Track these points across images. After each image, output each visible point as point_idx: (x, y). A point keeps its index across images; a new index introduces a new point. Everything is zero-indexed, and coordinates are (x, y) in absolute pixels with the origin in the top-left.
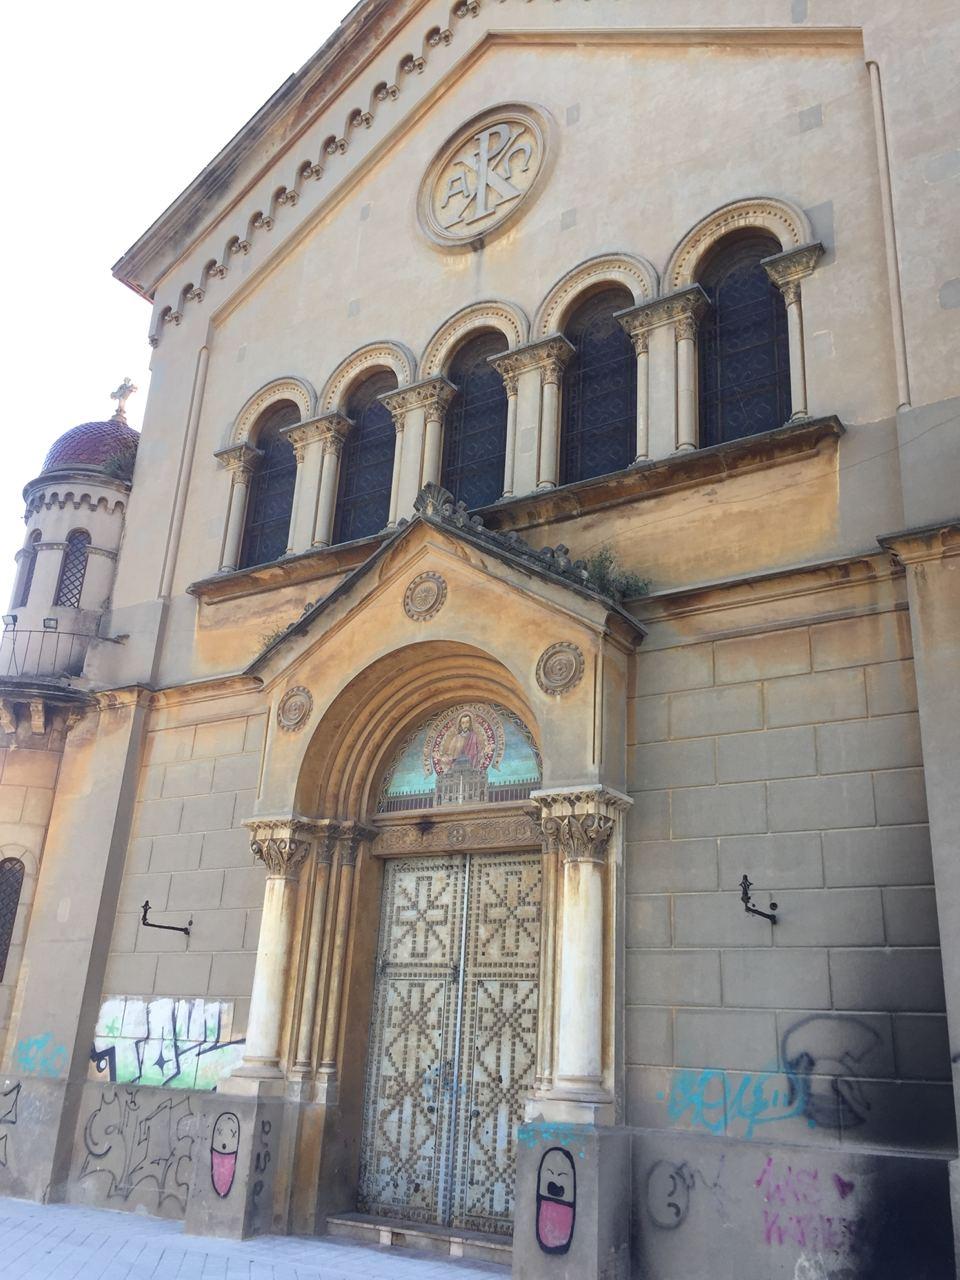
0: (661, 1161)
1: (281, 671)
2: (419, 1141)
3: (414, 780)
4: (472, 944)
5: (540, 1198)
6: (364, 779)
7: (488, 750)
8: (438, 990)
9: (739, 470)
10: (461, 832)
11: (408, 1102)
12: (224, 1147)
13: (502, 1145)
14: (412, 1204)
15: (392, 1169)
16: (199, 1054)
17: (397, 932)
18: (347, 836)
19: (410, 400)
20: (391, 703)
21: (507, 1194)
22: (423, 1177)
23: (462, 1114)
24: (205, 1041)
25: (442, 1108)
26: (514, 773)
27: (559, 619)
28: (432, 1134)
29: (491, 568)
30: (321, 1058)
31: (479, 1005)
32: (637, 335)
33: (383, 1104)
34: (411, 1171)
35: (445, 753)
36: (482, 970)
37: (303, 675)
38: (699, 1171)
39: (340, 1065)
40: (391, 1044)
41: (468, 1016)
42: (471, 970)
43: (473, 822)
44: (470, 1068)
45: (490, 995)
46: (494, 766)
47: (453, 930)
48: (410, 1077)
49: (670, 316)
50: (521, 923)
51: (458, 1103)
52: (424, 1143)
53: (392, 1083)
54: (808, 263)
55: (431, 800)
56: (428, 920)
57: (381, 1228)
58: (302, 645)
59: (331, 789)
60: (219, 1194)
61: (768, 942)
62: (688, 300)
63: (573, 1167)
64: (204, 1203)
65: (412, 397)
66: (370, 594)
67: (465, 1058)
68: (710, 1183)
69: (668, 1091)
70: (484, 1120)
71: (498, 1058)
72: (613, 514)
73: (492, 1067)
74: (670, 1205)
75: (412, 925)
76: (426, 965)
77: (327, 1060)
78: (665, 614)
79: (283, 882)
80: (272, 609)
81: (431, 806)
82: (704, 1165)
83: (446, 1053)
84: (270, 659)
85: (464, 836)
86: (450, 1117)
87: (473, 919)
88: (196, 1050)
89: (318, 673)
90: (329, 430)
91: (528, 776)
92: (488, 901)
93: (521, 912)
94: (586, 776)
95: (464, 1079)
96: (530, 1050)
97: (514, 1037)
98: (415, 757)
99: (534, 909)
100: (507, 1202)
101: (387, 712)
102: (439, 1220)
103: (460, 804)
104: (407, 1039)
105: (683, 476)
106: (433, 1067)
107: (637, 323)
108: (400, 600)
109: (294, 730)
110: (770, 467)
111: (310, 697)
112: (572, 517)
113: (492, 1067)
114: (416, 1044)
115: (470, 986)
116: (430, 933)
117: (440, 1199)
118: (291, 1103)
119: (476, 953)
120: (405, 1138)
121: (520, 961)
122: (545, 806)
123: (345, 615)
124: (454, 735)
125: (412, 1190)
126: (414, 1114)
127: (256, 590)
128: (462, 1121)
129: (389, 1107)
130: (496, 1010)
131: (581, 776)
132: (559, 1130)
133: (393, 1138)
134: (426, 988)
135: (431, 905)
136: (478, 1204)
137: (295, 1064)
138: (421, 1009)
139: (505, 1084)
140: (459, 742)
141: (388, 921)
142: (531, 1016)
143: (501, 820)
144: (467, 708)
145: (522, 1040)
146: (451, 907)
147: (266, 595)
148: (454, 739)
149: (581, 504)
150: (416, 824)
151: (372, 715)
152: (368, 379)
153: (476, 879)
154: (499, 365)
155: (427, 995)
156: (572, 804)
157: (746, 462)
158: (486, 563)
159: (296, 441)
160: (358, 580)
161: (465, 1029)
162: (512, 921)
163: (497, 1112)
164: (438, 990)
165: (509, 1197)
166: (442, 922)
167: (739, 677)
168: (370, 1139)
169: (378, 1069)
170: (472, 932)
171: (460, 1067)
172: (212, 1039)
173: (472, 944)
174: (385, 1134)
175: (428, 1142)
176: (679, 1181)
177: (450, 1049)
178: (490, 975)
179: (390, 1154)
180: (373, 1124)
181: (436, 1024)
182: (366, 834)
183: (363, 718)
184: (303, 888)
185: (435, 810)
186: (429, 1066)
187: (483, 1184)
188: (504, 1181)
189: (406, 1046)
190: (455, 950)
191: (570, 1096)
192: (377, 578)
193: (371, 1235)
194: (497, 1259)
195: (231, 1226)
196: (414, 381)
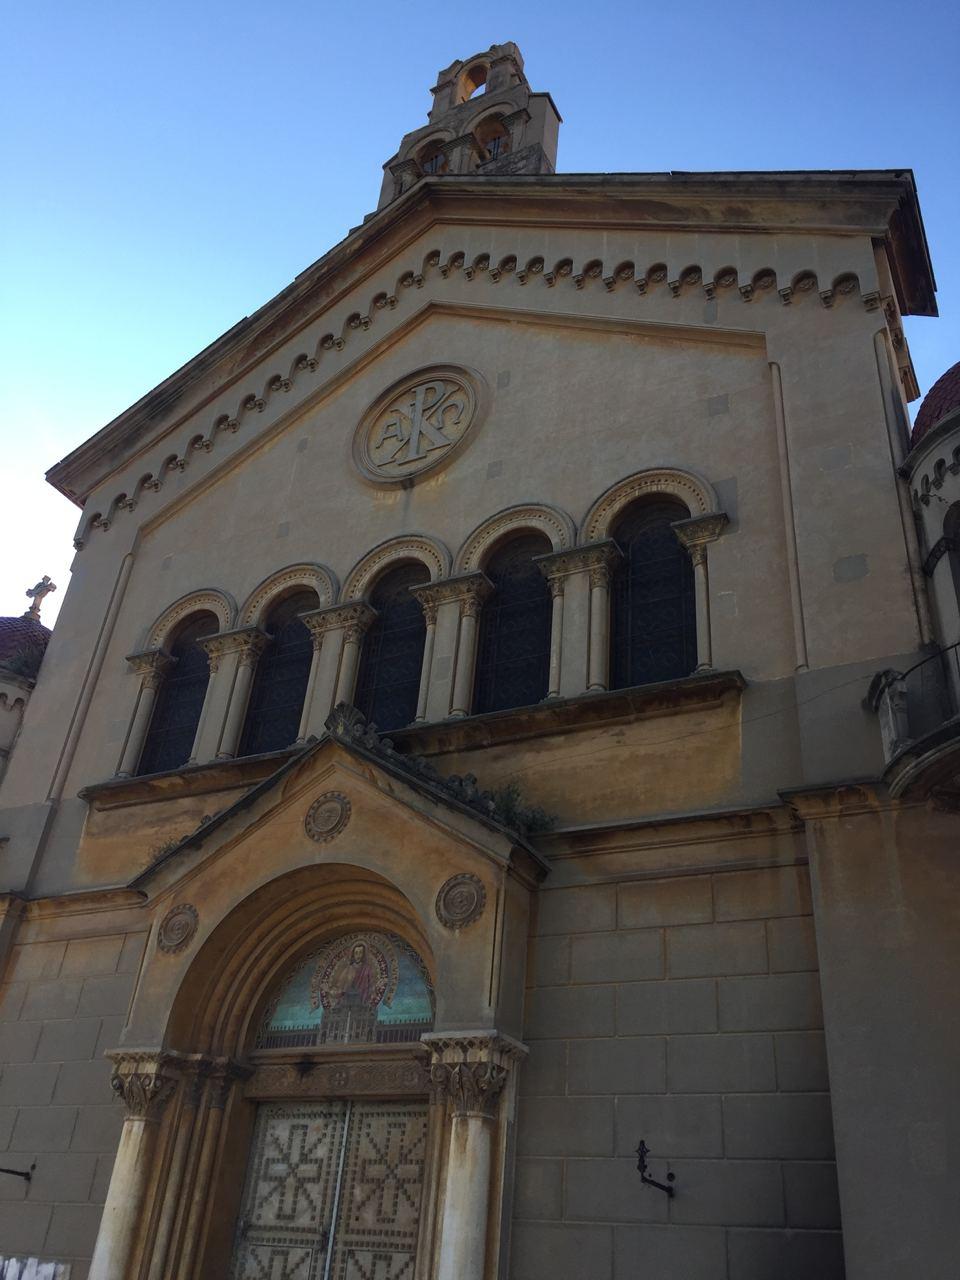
3: (299, 1015)
4: (345, 1206)
7: (380, 984)
8: (303, 1260)
10: (344, 1075)
17: (264, 1188)
18: (218, 1075)
35: (334, 985)
36: (354, 1238)
37: (192, 890)
42: (341, 1236)
43: (358, 1064)
47: (326, 1188)
50: (400, 1184)
54: (714, 530)
55: (315, 1036)
58: (199, 857)
62: (603, 551)
76: (292, 1229)
80: (168, 819)
81: (314, 1044)
87: (349, 1177)
90: (246, 642)
91: (421, 1015)
103: (346, 1043)
107: (554, 569)
110: (676, 714)
115: (339, 1256)
119: (349, 1217)
124: (345, 966)
140: (350, 975)
141: (254, 1175)
143: (387, 1064)
144: (362, 937)
146: (325, 1162)
150: (296, 1064)
151: (260, 940)
154: (420, 595)
155: (291, 1265)
159: (211, 651)
164: (303, 1260)
166: (314, 1179)
170: (347, 1192)
183: (251, 941)
185: (318, 1048)
190: (326, 1213)
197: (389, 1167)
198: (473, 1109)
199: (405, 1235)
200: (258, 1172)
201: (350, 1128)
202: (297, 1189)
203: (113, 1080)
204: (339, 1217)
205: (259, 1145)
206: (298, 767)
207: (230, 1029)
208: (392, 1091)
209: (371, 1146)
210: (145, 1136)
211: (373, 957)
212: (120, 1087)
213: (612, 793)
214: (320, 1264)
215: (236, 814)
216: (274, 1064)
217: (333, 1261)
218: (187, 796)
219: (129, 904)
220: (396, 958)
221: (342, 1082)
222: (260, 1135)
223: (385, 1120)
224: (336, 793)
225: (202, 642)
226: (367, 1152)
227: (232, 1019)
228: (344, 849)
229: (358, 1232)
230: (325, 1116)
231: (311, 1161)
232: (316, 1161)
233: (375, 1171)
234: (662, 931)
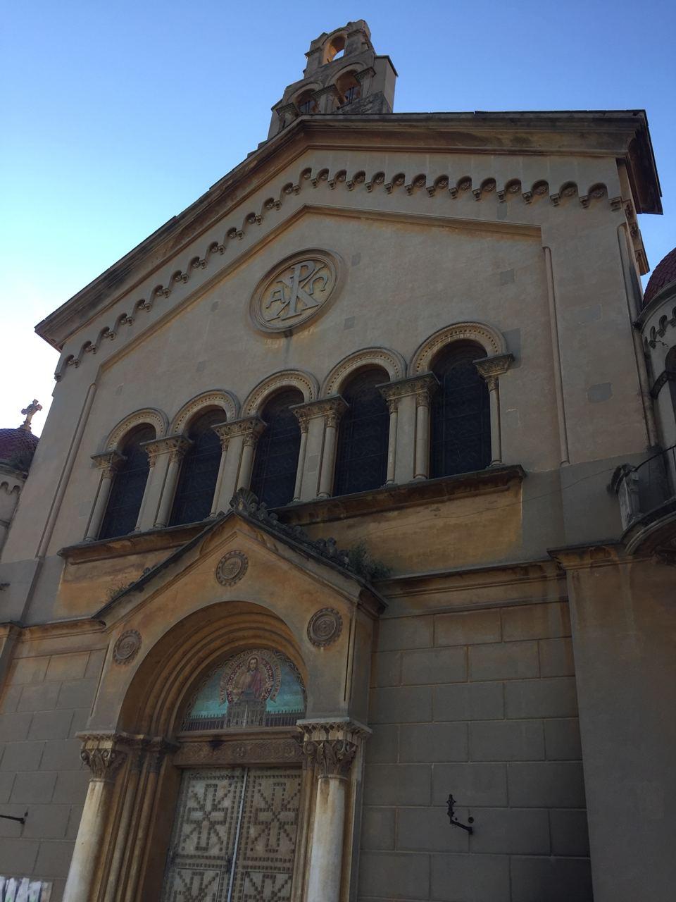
3: (212, 707)
4: (243, 842)
6: (173, 704)
7: (268, 685)
10: (243, 749)
17: (187, 828)
29: (281, 551)
31: (245, 892)
32: (391, 400)
35: (236, 686)
36: (250, 863)
42: (241, 862)
43: (253, 742)
46: (271, 699)
49: (413, 391)
50: (282, 825)
54: (503, 365)
58: (139, 598)
76: (207, 857)
81: (222, 727)
87: (246, 820)
90: (175, 446)
91: (296, 707)
107: (391, 393)
110: (476, 495)
112: (339, 519)
115: (239, 876)
119: (246, 849)
121: (279, 857)
141: (180, 819)
146: (229, 811)
150: (209, 741)
151: (185, 654)
152: (206, 414)
153: (251, 788)
154: (297, 412)
155: (205, 882)
170: (244, 831)
173: (243, 842)
182: (171, 748)
183: (177, 657)
185: (225, 730)
197: (274, 814)
198: (333, 773)
200: (183, 817)
201: (247, 786)
202: (210, 829)
203: (82, 753)
204: (239, 849)
206: (210, 534)
210: (104, 793)
213: (430, 551)
215: (167, 567)
217: (235, 879)
218: (134, 554)
221: (242, 754)
229: (252, 859)
233: (263, 816)
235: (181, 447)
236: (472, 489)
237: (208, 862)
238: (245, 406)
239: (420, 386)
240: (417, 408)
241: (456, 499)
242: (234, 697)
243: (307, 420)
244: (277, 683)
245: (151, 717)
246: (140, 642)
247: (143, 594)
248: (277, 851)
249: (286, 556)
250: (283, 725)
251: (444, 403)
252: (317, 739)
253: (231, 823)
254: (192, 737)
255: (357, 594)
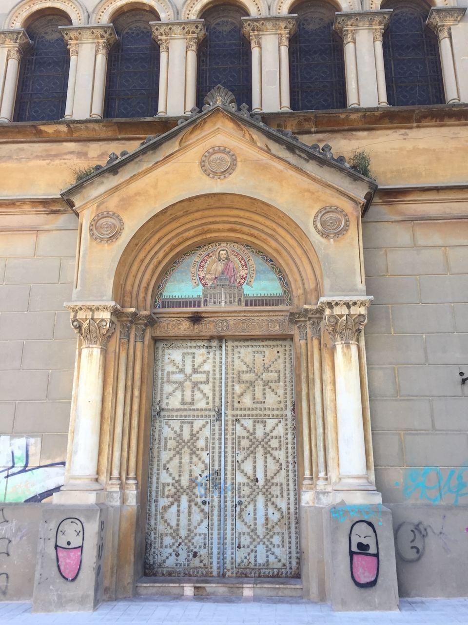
0: (404, 522)
1: (92, 197)
2: (195, 523)
3: (183, 287)
4: (229, 396)
5: (352, 554)
7: (243, 273)
8: (204, 426)
9: (421, 124)
10: (225, 324)
11: (184, 500)
12: (69, 543)
13: (261, 521)
14: (192, 565)
15: (173, 544)
16: (7, 477)
17: (168, 388)
18: (141, 322)
19: (175, 31)
20: (173, 234)
21: (267, 551)
22: (200, 547)
23: (229, 504)
24: (13, 467)
25: (212, 501)
26: (263, 289)
27: (329, 191)
28: (206, 518)
29: (273, 151)
30: (127, 474)
31: (237, 434)
32: (347, 30)
33: (163, 502)
34: (190, 544)
35: (208, 273)
36: (239, 412)
37: (112, 203)
38: (430, 526)
39: (140, 478)
40: (168, 462)
41: (229, 442)
42: (230, 412)
43: (235, 318)
44: (233, 474)
45: (245, 428)
46: (248, 284)
47: (214, 387)
48: (185, 482)
49: (371, 25)
50: (266, 383)
51: (225, 497)
52: (199, 525)
53: (170, 487)
54: (457, 17)
55: (199, 302)
56: (193, 380)
57: (184, 585)
58: (112, 181)
59: (128, 288)
60: (67, 579)
61: (460, 394)
62: (385, 18)
63: (375, 531)
64: (51, 587)
65: (178, 30)
66: (172, 154)
67: (229, 468)
68: (437, 532)
69: (402, 480)
70: (246, 507)
71: (255, 467)
72: (338, 135)
73: (250, 472)
74: (412, 548)
75: (181, 384)
76: (194, 410)
77: (132, 475)
78: (380, 201)
79: (99, 350)
80: (56, 156)
81: (199, 306)
82: (433, 522)
83: (213, 465)
84: (85, 188)
85: (228, 327)
86: (220, 506)
87: (230, 380)
88: (5, 474)
89: (127, 203)
90: (102, 37)
92: (240, 369)
93: (265, 376)
94: (357, 290)
95: (229, 482)
96: (278, 461)
97: (266, 453)
98: (184, 274)
99: (276, 375)
100: (267, 556)
101: (169, 241)
102: (215, 573)
103: (223, 307)
104: (181, 458)
105: (387, 120)
106: (204, 475)
107: (349, 23)
108: (197, 162)
109: (107, 242)
110: (442, 126)
111: (121, 220)
112: (309, 132)
113: (250, 472)
114: (188, 461)
115: (230, 423)
116: (196, 389)
117: (215, 560)
118: (112, 507)
119: (233, 402)
120: (184, 521)
121: (267, 407)
122: (329, 308)
123: (151, 165)
125: (191, 556)
126: (190, 507)
127: (40, 139)
128: (229, 508)
129: (169, 504)
130: (251, 437)
131: (353, 290)
132: (359, 509)
133: (173, 523)
134: (194, 425)
135: (195, 371)
136: (245, 560)
137: (111, 479)
138: (192, 439)
139: (261, 482)
140: (220, 267)
141: (160, 381)
142: (277, 440)
143: (256, 318)
145: (271, 455)
146: (211, 373)
147: (48, 144)
148: (215, 264)
149: (316, 125)
150: (188, 318)
151: (159, 240)
152: (128, 11)
153: (230, 355)
154: (249, 25)
155: (196, 429)
156: (348, 307)
157: (427, 120)
158: (270, 147)
159: (71, 39)
160: (165, 142)
161: (228, 450)
162: (260, 382)
163: (256, 501)
164: (204, 426)
165: (269, 553)
166: (205, 382)
167: (430, 243)
168: (153, 526)
169: (158, 479)
170: (230, 389)
171: (226, 474)
172: (20, 465)
173: (229, 396)
174: (166, 521)
175: (202, 524)
176: (416, 532)
177: (216, 463)
178: (245, 416)
179: (171, 534)
180: (156, 515)
181: (204, 448)
182: (151, 322)
183: (153, 241)
184: (111, 356)
185: (202, 309)
186: (200, 475)
187: (248, 547)
188: (264, 543)
189: (180, 463)
190: (217, 400)
191: (363, 488)
192: (177, 143)
193: (176, 591)
194: (280, 594)
195: (82, 601)
196: (178, 19)
197: (257, 375)
198: (352, 340)
199: (273, 409)
200: (162, 379)
201: (226, 354)
202: (193, 388)
203: (73, 322)
204: (226, 402)
205: (160, 364)
206: (193, 126)
207: (141, 295)
208: (260, 333)
209: (242, 363)
210: (101, 358)
211: (236, 259)
212: (79, 328)
213: (403, 169)
214: (217, 428)
215: (145, 153)
216: (172, 317)
217: (226, 425)
218: (71, 141)
219: (37, 211)
220: (251, 258)
221: (225, 328)
222: (160, 359)
223: (250, 350)
224: (222, 148)
225: (64, 30)
226: (240, 367)
227: (142, 289)
228: (236, 183)
229: (241, 409)
230: (207, 347)
231: (201, 372)
232: (204, 372)
233: (246, 377)
234: (443, 248)
235: (108, 40)
236: (438, 121)
237: (196, 413)
238: (184, 9)
239: (378, 22)
240: (187, 52)
241: (424, 127)
242: (207, 281)
243: (258, 35)
244: (252, 272)
245: (131, 293)
246: (122, 224)
247: (116, 177)
248: (264, 402)
249: (281, 156)
250: (263, 305)
251: (208, 52)
252: (340, 314)
253: (214, 383)
254: (169, 313)
255: (363, 195)
